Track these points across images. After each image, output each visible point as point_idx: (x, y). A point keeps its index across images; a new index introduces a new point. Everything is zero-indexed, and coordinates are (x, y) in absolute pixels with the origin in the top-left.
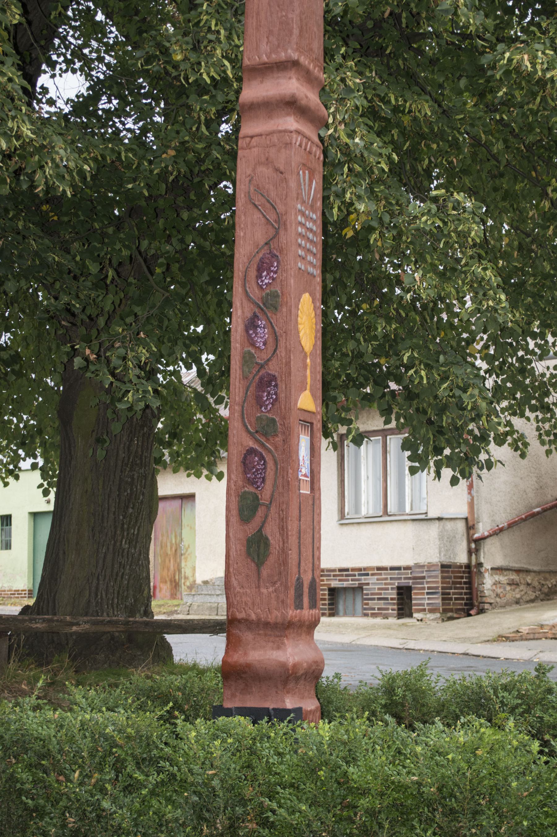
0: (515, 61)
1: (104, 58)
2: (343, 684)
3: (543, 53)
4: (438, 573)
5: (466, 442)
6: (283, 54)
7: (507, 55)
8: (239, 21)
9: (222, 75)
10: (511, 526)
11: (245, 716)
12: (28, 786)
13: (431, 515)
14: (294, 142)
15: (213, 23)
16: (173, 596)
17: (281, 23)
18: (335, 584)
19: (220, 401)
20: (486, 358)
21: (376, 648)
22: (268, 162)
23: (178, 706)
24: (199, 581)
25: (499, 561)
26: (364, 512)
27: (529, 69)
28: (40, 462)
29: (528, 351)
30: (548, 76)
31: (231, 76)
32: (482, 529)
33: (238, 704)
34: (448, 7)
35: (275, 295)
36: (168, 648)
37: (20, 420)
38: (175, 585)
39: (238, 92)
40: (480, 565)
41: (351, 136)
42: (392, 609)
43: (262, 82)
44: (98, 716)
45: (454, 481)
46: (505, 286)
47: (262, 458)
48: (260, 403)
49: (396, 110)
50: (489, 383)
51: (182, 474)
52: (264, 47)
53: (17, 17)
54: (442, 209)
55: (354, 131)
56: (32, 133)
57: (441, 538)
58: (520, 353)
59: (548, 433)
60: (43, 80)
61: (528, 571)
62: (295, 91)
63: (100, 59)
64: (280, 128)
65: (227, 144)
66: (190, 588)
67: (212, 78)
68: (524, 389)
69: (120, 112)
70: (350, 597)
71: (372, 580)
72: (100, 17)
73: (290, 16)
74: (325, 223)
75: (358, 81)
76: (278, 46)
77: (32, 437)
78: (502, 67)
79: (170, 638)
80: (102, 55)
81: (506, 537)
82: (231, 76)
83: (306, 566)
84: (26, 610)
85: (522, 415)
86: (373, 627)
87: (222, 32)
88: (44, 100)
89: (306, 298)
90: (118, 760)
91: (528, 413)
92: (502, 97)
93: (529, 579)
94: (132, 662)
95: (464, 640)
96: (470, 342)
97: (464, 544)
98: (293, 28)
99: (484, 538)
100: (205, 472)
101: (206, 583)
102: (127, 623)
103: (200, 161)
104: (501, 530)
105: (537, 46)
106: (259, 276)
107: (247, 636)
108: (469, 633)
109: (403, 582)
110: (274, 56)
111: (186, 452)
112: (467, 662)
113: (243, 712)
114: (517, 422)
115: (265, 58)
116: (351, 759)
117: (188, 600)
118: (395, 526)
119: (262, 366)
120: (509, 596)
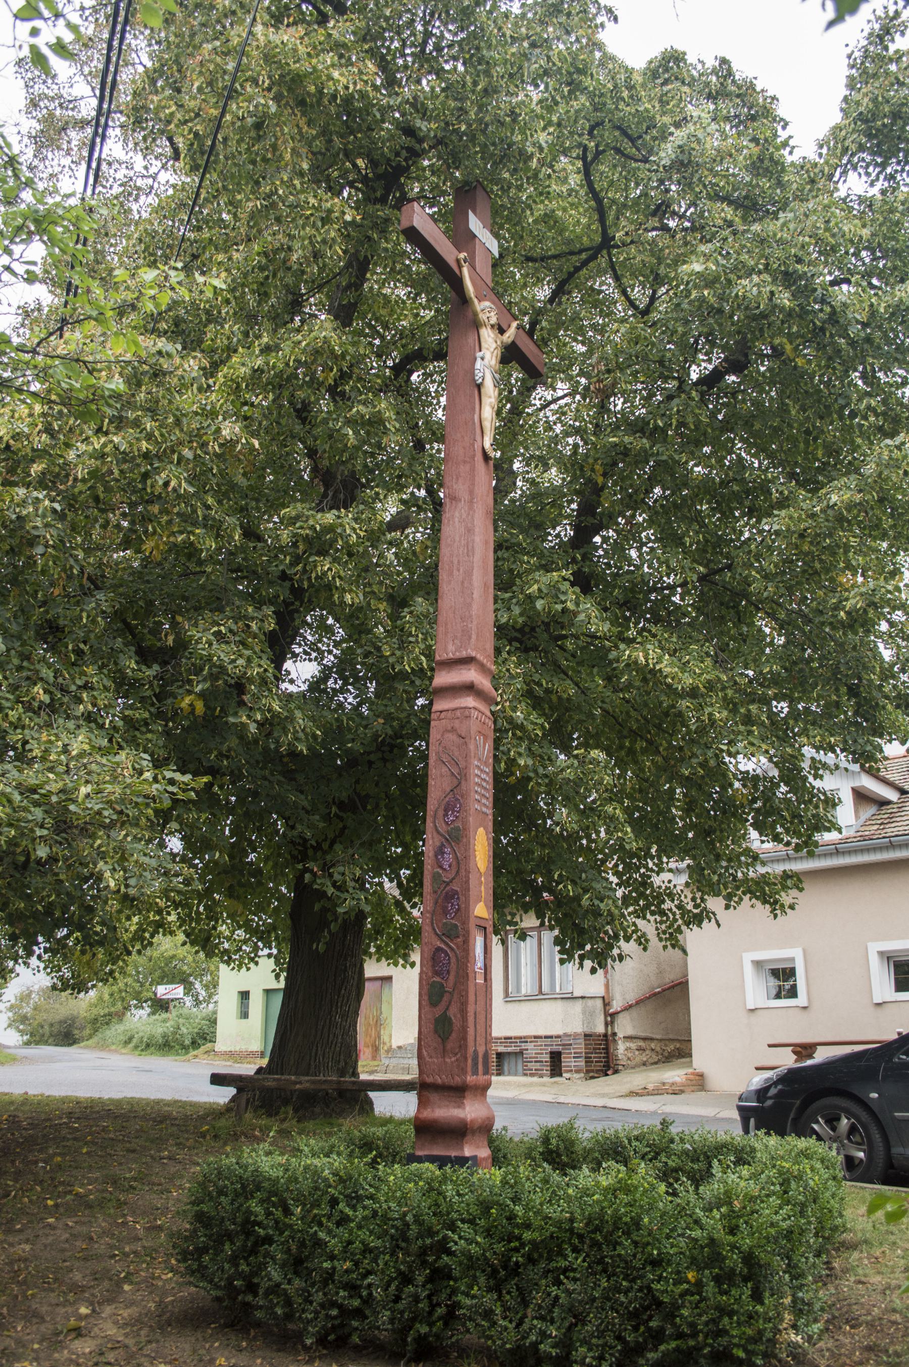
2: (509, 1134)
4: (582, 1041)
5: (603, 940)
10: (638, 1003)
11: (432, 1162)
12: (260, 1218)
13: (576, 994)
16: (374, 1058)
18: (501, 1049)
19: (414, 906)
20: (617, 873)
21: (534, 1102)
22: (453, 730)
23: (380, 1155)
24: (394, 1046)
25: (630, 1031)
26: (523, 992)
28: (275, 951)
29: (648, 869)
32: (616, 1006)
33: (426, 1153)
35: (457, 829)
36: (370, 1103)
37: (260, 919)
38: (376, 1049)
39: (431, 679)
40: (614, 1034)
41: (514, 709)
42: (546, 1070)
44: (316, 1162)
45: (593, 971)
46: (631, 821)
47: (447, 954)
48: (445, 912)
49: (548, 691)
50: (619, 893)
51: (384, 962)
52: (451, 647)
54: (582, 763)
57: (584, 1013)
58: (642, 870)
59: (664, 932)
60: (288, 665)
61: (652, 1039)
63: (330, 652)
66: (388, 1051)
68: (646, 898)
69: (342, 690)
70: (513, 1060)
71: (530, 1046)
72: (330, 621)
74: (495, 773)
77: (269, 932)
79: (371, 1094)
81: (634, 1012)
83: (481, 1040)
84: (260, 1071)
85: (644, 918)
86: (531, 1084)
89: (481, 831)
90: (333, 1197)
91: (648, 916)
93: (653, 1045)
94: (341, 1114)
95: (603, 1095)
96: (604, 862)
97: (602, 1017)
99: (617, 1013)
100: (401, 961)
101: (400, 1048)
102: (339, 1082)
103: (402, 727)
104: (631, 1006)
106: (446, 815)
107: (434, 1097)
108: (607, 1090)
109: (555, 1048)
111: (387, 945)
112: (606, 1114)
113: (432, 1159)
114: (640, 923)
115: (451, 656)
116: (516, 1199)
117: (386, 1062)
118: (548, 1003)
119: (448, 884)
120: (638, 1060)
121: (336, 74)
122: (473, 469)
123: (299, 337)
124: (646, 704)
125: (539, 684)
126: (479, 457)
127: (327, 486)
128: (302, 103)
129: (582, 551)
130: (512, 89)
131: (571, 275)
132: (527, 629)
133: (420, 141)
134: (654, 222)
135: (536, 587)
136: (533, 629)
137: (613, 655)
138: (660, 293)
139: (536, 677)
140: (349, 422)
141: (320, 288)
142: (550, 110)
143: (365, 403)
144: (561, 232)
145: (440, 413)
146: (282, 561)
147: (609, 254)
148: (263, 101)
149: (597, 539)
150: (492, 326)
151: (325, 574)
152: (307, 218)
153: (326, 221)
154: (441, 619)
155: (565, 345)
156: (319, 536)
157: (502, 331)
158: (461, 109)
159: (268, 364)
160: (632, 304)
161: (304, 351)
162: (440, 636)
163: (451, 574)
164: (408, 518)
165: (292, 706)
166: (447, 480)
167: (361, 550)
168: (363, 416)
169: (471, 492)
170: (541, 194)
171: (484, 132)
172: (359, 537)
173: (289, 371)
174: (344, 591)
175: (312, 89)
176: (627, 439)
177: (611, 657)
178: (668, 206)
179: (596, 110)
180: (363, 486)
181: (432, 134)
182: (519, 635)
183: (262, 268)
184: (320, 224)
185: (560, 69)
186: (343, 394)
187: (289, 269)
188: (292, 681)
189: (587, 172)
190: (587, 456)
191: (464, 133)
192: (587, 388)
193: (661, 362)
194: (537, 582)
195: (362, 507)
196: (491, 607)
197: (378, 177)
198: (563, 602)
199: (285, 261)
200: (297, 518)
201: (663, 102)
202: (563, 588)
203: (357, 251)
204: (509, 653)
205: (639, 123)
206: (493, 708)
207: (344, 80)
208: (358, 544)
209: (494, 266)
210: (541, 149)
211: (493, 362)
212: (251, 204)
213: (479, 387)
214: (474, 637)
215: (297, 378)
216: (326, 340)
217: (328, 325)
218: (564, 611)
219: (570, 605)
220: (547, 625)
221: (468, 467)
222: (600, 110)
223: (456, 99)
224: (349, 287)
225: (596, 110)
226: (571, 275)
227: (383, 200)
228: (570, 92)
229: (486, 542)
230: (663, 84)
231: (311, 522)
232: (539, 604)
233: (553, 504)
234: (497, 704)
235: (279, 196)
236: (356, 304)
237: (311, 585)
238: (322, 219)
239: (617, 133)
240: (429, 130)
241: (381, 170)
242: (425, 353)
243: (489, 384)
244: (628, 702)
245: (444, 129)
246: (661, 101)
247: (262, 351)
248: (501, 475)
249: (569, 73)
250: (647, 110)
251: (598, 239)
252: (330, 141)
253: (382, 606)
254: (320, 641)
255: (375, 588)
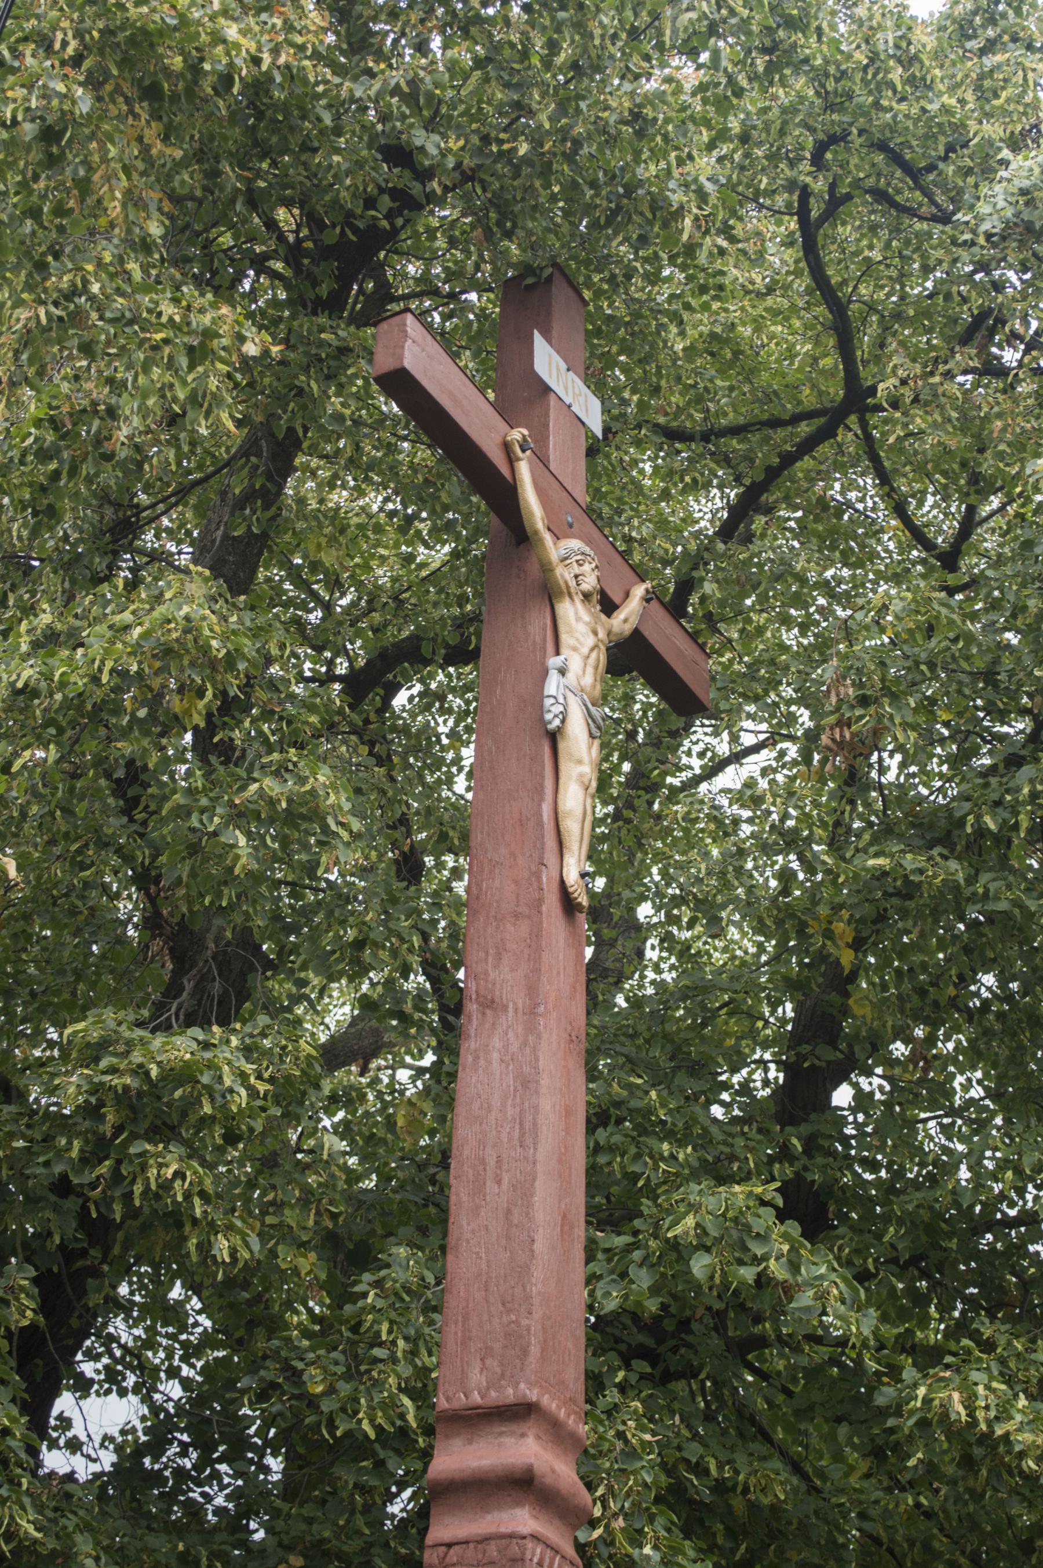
0: (937, 1402)
1: (179, 1368)
3: (988, 1387)
6: (511, 1391)
7: (922, 1391)
8: (431, 1323)
9: (399, 1423)
14: (528, 1556)
15: (385, 1327)
17: (507, 1335)
27: (964, 1418)
30: (999, 1432)
31: (414, 1425)
34: (811, 1303)
39: (426, 1455)
41: (636, 1538)
43: (470, 1442)
49: (721, 1488)
52: (476, 1377)
53: (29, 1313)
55: (640, 1532)
56: (37, 1529)
60: (65, 1403)
62: (532, 1460)
63: (173, 1373)
64: (503, 1530)
65: (402, 1544)
67: (379, 1429)
73: (524, 1322)
75: (648, 1437)
76: (502, 1376)
78: (912, 1413)
80: (176, 1363)
82: (414, 1425)
87: (401, 1343)
88: (62, 1442)
92: (915, 1467)
98: (529, 1343)
105: (975, 1376)
110: (493, 1394)
115: (476, 1398)
121: (232, 32)
122: (537, 935)
123: (127, 617)
124: (975, 1527)
125: (701, 1470)
126: (552, 903)
127: (182, 961)
128: (151, 93)
129: (805, 1129)
130: (636, 63)
131: (773, 474)
132: (669, 1325)
133: (425, 175)
134: (965, 357)
135: (690, 1221)
136: (684, 1325)
137: (886, 1395)
138: (985, 510)
139: (693, 1451)
140: (239, 816)
141: (182, 493)
142: (723, 106)
143: (280, 772)
144: (750, 374)
145: (460, 784)
146: (61, 1153)
147: (864, 425)
148: (61, 88)
149: (842, 1096)
150: (587, 596)
151: (166, 1186)
152: (156, 348)
153: (197, 355)
154: (453, 1303)
155: (760, 631)
156: (154, 1089)
157: (609, 607)
158: (518, 105)
159: (49, 678)
160: (918, 535)
161: (136, 650)
162: (451, 1346)
163: (479, 1190)
164: (377, 1033)
165: (70, 1522)
166: (473, 956)
167: (258, 1126)
168: (272, 802)
169: (532, 990)
170: (703, 289)
171: (570, 158)
172: (253, 1093)
173: (99, 694)
174: (213, 1228)
175: (177, 62)
176: (910, 862)
177: (880, 1401)
178: (1001, 321)
179: (830, 107)
180: (269, 965)
181: (451, 162)
182: (650, 1342)
183: (44, 455)
184: (184, 362)
185: (746, 22)
186: (226, 751)
187: (109, 457)
188: (74, 1446)
189: (811, 250)
190: (813, 896)
191: (526, 160)
192: (812, 737)
193: (989, 676)
194: (694, 1208)
195: (263, 1020)
196: (579, 1272)
197: (325, 252)
198: (756, 1260)
199: (99, 441)
200: (102, 1046)
201: (985, 92)
202: (758, 1225)
203: (272, 416)
204: (622, 1388)
205: (929, 137)
206: (582, 1536)
207: (248, 44)
208: (251, 1112)
209: (592, 452)
210: (702, 196)
211: (588, 680)
212: (23, 314)
213: (554, 737)
214: (535, 1350)
215: (118, 710)
216: (190, 626)
217: (196, 588)
218: (763, 1281)
219: (777, 1269)
220: (720, 1317)
221: (524, 928)
222: (840, 108)
223: (507, 85)
224: (247, 498)
225: (830, 107)
226: (773, 474)
227: (334, 305)
228: (770, 67)
229: (568, 1112)
230: (983, 52)
231: (137, 1057)
232: (700, 1265)
233: (733, 1008)
234: (593, 1524)
235: (92, 298)
236: (264, 536)
237: (130, 1212)
238: (191, 350)
239: (879, 158)
240: (443, 154)
241: (331, 237)
242: (426, 650)
243: (577, 730)
244: (929, 1515)
245: (479, 151)
246: (978, 88)
247: (36, 645)
248: (607, 933)
249: (769, 30)
250: (945, 110)
251: (837, 391)
252: (214, 174)
253: (307, 1263)
254: (150, 1343)
255: (290, 1217)
